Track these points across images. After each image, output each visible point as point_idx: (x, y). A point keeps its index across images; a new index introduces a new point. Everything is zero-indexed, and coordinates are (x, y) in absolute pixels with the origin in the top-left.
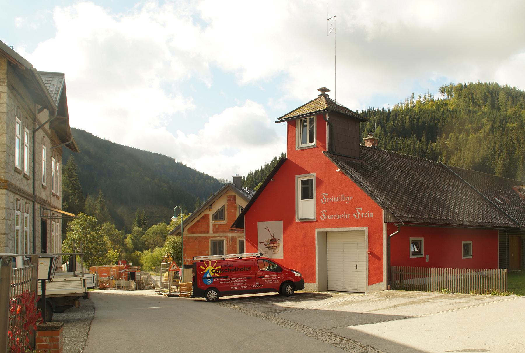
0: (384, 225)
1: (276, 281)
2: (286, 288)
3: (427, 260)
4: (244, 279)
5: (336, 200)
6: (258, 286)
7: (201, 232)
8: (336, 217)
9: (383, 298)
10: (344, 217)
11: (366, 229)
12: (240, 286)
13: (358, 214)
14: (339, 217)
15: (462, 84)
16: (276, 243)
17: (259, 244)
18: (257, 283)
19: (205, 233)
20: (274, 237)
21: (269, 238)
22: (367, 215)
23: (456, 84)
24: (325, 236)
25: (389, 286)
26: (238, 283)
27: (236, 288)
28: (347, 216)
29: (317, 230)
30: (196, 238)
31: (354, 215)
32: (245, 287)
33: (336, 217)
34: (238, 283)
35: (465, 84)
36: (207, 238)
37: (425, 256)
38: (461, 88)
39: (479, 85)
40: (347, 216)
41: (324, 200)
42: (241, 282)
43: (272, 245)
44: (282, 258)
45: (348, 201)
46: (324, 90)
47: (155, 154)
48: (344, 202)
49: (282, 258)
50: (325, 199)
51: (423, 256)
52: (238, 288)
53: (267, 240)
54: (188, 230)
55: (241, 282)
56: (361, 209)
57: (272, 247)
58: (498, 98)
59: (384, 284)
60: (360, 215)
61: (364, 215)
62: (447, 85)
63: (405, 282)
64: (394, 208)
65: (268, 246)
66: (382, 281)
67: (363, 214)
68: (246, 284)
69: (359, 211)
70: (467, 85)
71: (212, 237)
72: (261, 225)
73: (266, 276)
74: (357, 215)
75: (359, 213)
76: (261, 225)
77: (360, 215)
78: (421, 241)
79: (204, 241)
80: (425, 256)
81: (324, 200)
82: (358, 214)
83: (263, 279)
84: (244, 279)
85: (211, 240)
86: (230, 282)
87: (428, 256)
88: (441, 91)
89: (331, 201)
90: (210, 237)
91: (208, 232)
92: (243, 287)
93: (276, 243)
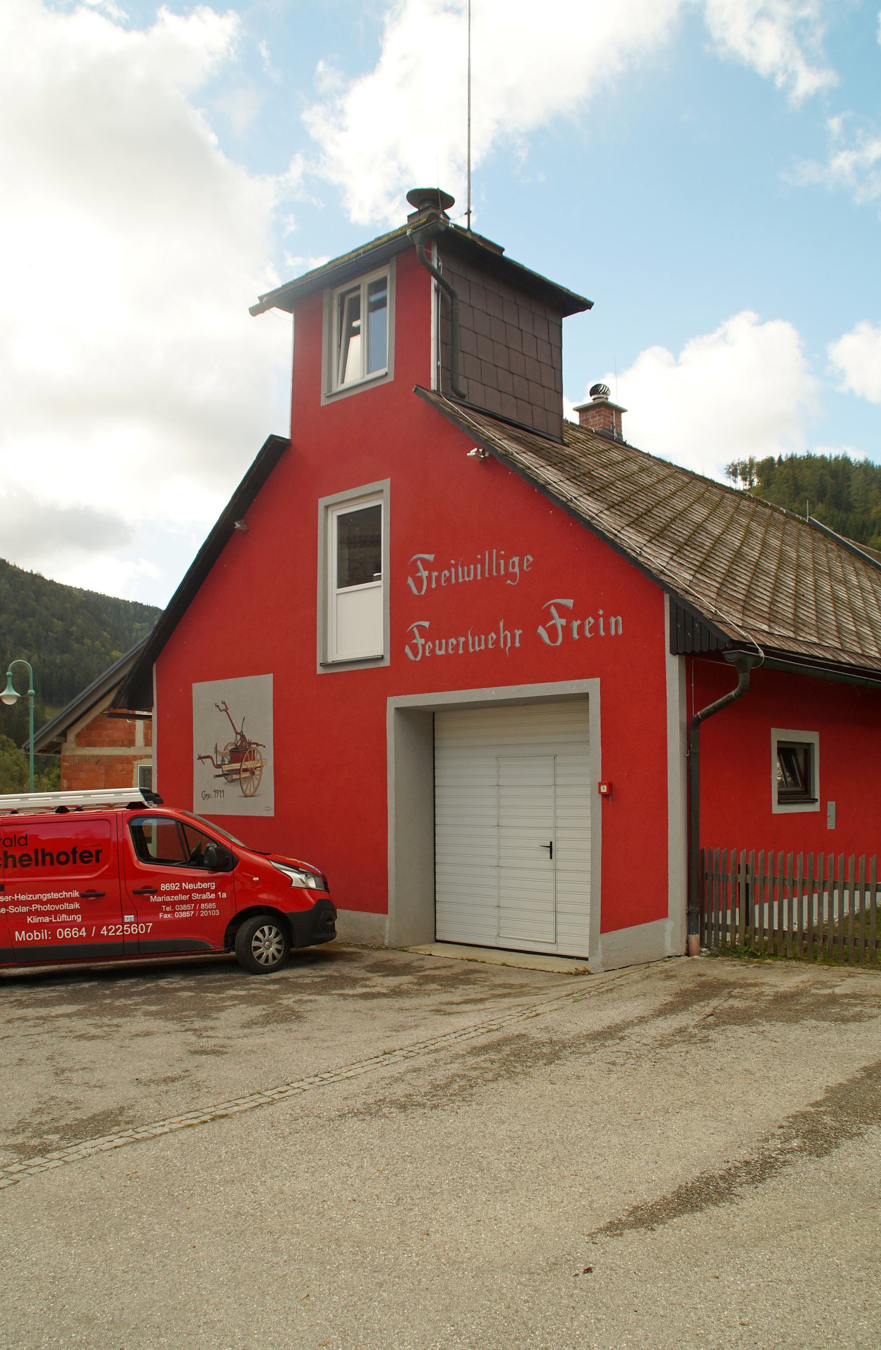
0: (673, 666)
1: (209, 910)
2: (250, 937)
3: (831, 824)
4: (71, 900)
5: (466, 574)
6: (134, 929)
7: (113, 743)
8: (466, 644)
9: (686, 1019)
10: (496, 642)
11: (592, 686)
12: (52, 927)
13: (558, 624)
14: (477, 645)
15: (772, 459)
16: (251, 757)
17: (197, 763)
18: (129, 918)
19: (123, 745)
20: (243, 737)
21: (229, 739)
22: (594, 628)
23: (760, 458)
24: (426, 726)
25: (695, 939)
26: (48, 913)
27: (36, 936)
28: (510, 638)
29: (394, 702)
30: (98, 760)
31: (541, 631)
32: (74, 933)
33: (466, 644)
34: (48, 913)
35: (780, 458)
36: (128, 761)
37: (824, 807)
38: (767, 468)
39: (809, 461)
40: (510, 638)
41: (418, 582)
42: (56, 913)
43: (237, 766)
44: (271, 814)
45: (513, 576)
46: (430, 201)
47: (136, 604)
48: (501, 579)
49: (271, 814)
50: (425, 578)
51: (815, 808)
52: (44, 935)
53: (221, 749)
54: (78, 736)
55: (56, 913)
56: (569, 603)
57: (237, 772)
58: (849, 486)
59: (670, 930)
60: (567, 629)
61: (581, 628)
62: (742, 460)
63: (765, 916)
64: (714, 596)
65: (227, 768)
66: (662, 912)
67: (576, 624)
68: (79, 918)
69: (563, 611)
70: (784, 459)
71: (141, 757)
72: (205, 694)
73: (164, 887)
74: (552, 632)
75: (560, 622)
76: (205, 694)
77: (567, 629)
78: (807, 748)
79: (119, 767)
80: (824, 807)
81: (418, 582)
82: (558, 624)
83: (154, 899)
84: (71, 900)
85: (139, 764)
86: (12, 909)
87: (831, 806)
88: (729, 473)
89: (448, 580)
90: (135, 758)
91: (131, 743)
92: (65, 933)
93: (251, 757)
